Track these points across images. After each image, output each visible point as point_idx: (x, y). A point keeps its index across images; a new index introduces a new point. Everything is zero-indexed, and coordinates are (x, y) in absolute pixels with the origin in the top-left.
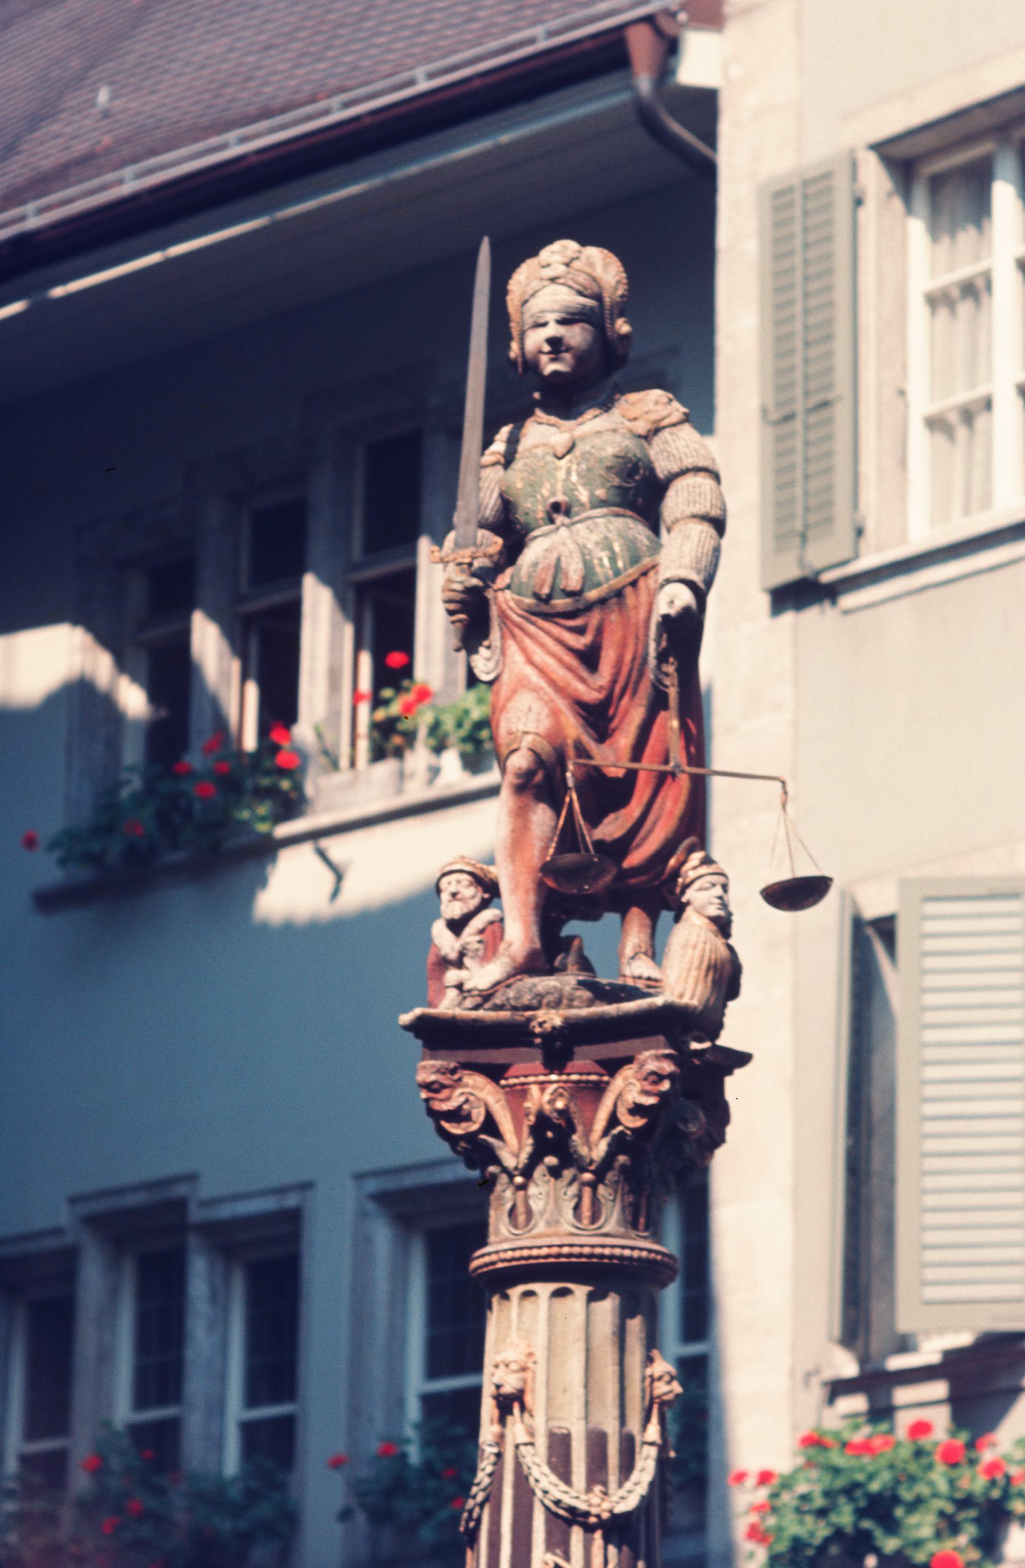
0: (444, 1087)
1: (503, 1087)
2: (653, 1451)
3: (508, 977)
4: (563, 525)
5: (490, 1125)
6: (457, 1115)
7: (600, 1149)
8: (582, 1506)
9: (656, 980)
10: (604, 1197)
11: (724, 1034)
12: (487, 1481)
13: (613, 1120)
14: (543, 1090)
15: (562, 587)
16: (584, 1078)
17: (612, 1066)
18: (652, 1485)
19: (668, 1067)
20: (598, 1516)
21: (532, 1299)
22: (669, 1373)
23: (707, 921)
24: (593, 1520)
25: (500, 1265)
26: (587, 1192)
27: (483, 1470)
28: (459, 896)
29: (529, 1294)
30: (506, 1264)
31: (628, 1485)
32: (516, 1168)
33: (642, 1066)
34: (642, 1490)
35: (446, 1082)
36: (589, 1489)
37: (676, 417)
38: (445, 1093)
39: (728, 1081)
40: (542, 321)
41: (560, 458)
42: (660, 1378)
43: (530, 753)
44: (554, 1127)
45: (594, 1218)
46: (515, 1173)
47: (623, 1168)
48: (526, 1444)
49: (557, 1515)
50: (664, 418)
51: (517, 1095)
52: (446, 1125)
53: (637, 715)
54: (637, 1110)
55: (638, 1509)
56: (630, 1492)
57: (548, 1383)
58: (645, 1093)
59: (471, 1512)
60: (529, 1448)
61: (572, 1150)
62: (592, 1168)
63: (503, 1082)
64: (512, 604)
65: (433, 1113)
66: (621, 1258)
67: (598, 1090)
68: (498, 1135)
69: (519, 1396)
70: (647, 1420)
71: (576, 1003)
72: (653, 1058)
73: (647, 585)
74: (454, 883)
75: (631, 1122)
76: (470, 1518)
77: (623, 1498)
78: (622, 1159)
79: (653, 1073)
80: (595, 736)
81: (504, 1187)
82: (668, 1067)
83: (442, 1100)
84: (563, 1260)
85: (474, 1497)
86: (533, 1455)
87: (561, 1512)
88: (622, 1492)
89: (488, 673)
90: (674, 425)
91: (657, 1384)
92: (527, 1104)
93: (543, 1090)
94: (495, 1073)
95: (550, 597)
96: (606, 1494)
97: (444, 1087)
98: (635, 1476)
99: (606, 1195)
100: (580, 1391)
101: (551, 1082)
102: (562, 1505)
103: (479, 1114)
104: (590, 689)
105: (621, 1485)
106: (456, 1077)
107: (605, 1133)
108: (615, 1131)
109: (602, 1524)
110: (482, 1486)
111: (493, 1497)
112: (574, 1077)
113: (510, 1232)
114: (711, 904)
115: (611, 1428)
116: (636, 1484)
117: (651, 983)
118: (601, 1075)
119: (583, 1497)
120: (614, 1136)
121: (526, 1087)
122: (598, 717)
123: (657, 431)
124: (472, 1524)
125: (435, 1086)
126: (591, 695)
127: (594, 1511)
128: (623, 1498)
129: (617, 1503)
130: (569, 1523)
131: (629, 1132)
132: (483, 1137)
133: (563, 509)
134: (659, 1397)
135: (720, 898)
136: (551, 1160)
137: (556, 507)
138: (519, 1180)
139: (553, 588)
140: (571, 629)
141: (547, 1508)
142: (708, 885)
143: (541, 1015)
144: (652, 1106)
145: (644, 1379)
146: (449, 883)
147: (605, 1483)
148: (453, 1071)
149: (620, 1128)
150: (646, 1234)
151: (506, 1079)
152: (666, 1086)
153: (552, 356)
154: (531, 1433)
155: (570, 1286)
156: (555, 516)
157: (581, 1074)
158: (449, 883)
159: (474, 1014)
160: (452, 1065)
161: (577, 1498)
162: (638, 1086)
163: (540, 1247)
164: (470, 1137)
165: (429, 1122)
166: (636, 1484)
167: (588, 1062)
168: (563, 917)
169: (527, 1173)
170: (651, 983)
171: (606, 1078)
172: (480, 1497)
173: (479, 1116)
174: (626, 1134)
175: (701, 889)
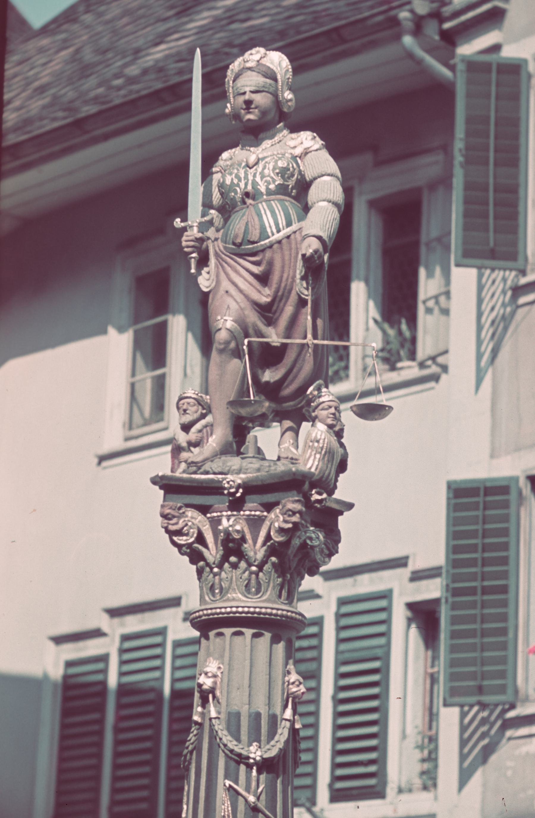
0: (174, 517)
1: (208, 518)
2: (288, 724)
3: (213, 457)
4: (251, 204)
5: (201, 539)
6: (179, 533)
7: (260, 555)
8: (244, 753)
9: (296, 460)
10: (263, 581)
11: (337, 491)
12: (193, 739)
13: (268, 537)
14: (228, 520)
15: (248, 239)
16: (253, 513)
17: (269, 507)
18: (287, 742)
19: (298, 507)
20: (254, 759)
21: (222, 637)
22: (298, 680)
23: (326, 427)
24: (252, 761)
25: (204, 618)
26: (253, 576)
27: (193, 732)
28: (187, 412)
29: (220, 634)
30: (207, 617)
31: (273, 743)
32: (214, 563)
33: (284, 506)
34: (280, 745)
35: (177, 514)
36: (250, 745)
37: (317, 146)
38: (174, 521)
39: (340, 518)
40: (242, 91)
41: (250, 168)
42: (293, 683)
43: (227, 331)
44: (234, 540)
45: (258, 591)
46: (213, 566)
47: (273, 564)
48: (215, 718)
49: (231, 758)
50: (311, 147)
51: (215, 523)
52: (175, 538)
53: (289, 310)
54: (281, 530)
55: (277, 756)
56: (273, 746)
57: (228, 685)
58: (285, 521)
59: (186, 756)
60: (217, 720)
61: (245, 554)
62: (256, 563)
63: (208, 515)
64: (222, 249)
65: (167, 531)
66: (287, 617)
67: (261, 520)
68: (206, 546)
69: (212, 690)
70: (286, 706)
71: (249, 471)
72: (292, 502)
73: (296, 239)
74: (186, 404)
75: (277, 538)
76: (185, 761)
77: (269, 749)
78: (274, 559)
79: (290, 510)
80: (266, 322)
81: (207, 574)
82: (298, 507)
83: (173, 524)
84: (262, 616)
85: (187, 748)
86: (219, 725)
87: (233, 756)
88: (268, 747)
89: (207, 287)
90: (317, 150)
91: (291, 686)
92: (220, 528)
93: (228, 520)
94: (204, 510)
95: (241, 244)
96: (260, 747)
97: (174, 517)
98: (277, 738)
99: (264, 579)
100: (247, 689)
101: (233, 515)
102: (234, 752)
103: (193, 533)
104: (264, 296)
105: (268, 742)
106: (181, 511)
107: (264, 544)
108: (269, 544)
109: (256, 763)
110: (192, 741)
111: (198, 749)
112: (247, 513)
113: (210, 599)
114: (329, 418)
115: (263, 711)
116: (277, 742)
117: (294, 461)
118: (263, 512)
119: (246, 749)
120: (268, 546)
121: (220, 518)
122: (267, 312)
123: (306, 153)
124: (186, 763)
125: (170, 516)
126: (265, 300)
127: (252, 755)
128: (269, 749)
129: (266, 752)
130: (238, 763)
131: (276, 544)
132: (196, 545)
133: (251, 195)
134: (293, 693)
135: (334, 414)
136: (233, 559)
137: (247, 194)
138: (216, 570)
139: (243, 239)
140: (253, 263)
141: (226, 755)
142: (326, 407)
143: (230, 477)
144: (289, 529)
145: (284, 683)
146: (183, 404)
147: (259, 741)
148: (180, 508)
149: (272, 541)
150: (287, 602)
151: (210, 513)
152: (296, 518)
153: (246, 111)
154: (219, 713)
155: (243, 630)
156: (247, 200)
157: (251, 511)
158: (183, 404)
159: (181, 475)
160: (179, 505)
161: (242, 749)
162: (281, 518)
163: (226, 608)
164: (189, 546)
165: (167, 536)
166: (277, 742)
167: (255, 504)
168: (250, 425)
169: (220, 566)
170: (294, 461)
171: (265, 514)
172: (190, 748)
173: (194, 532)
174: (275, 545)
175: (323, 409)
